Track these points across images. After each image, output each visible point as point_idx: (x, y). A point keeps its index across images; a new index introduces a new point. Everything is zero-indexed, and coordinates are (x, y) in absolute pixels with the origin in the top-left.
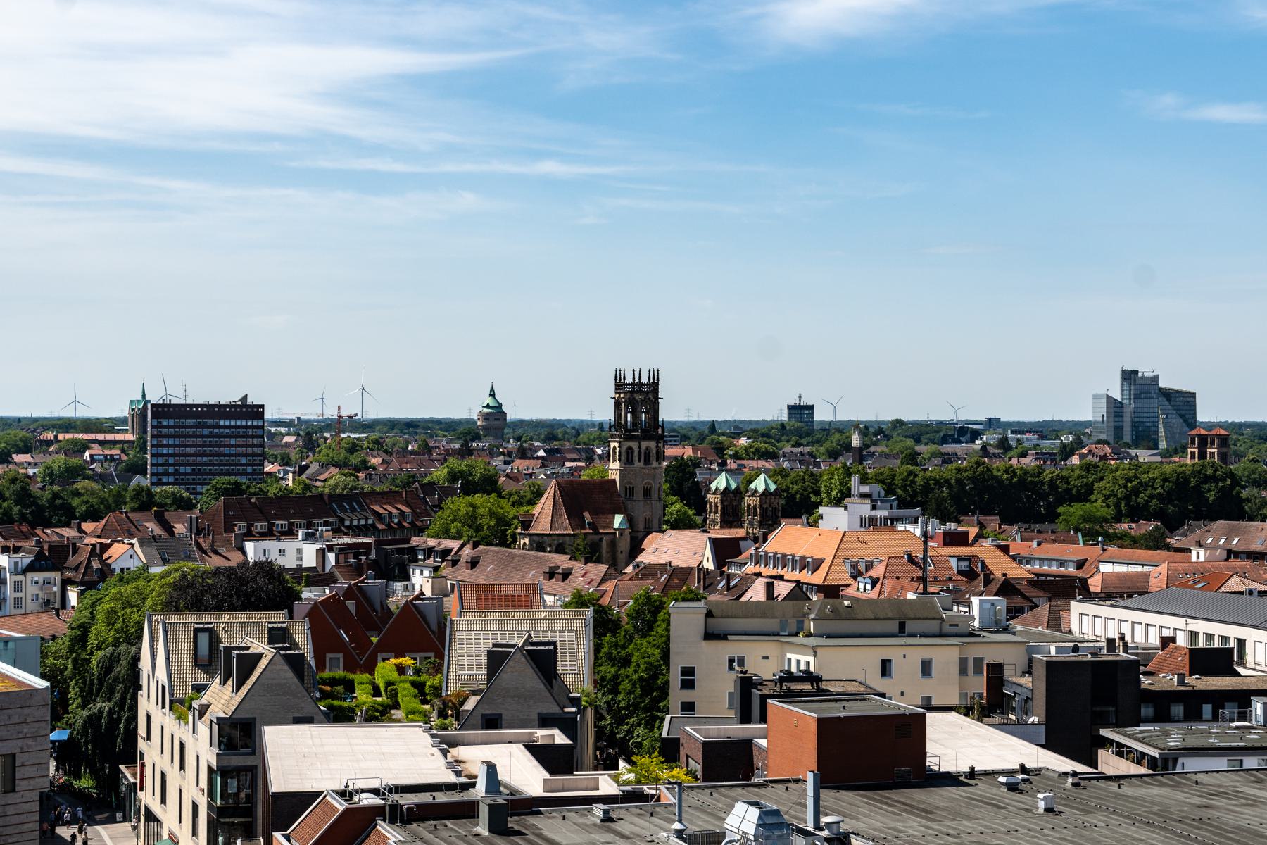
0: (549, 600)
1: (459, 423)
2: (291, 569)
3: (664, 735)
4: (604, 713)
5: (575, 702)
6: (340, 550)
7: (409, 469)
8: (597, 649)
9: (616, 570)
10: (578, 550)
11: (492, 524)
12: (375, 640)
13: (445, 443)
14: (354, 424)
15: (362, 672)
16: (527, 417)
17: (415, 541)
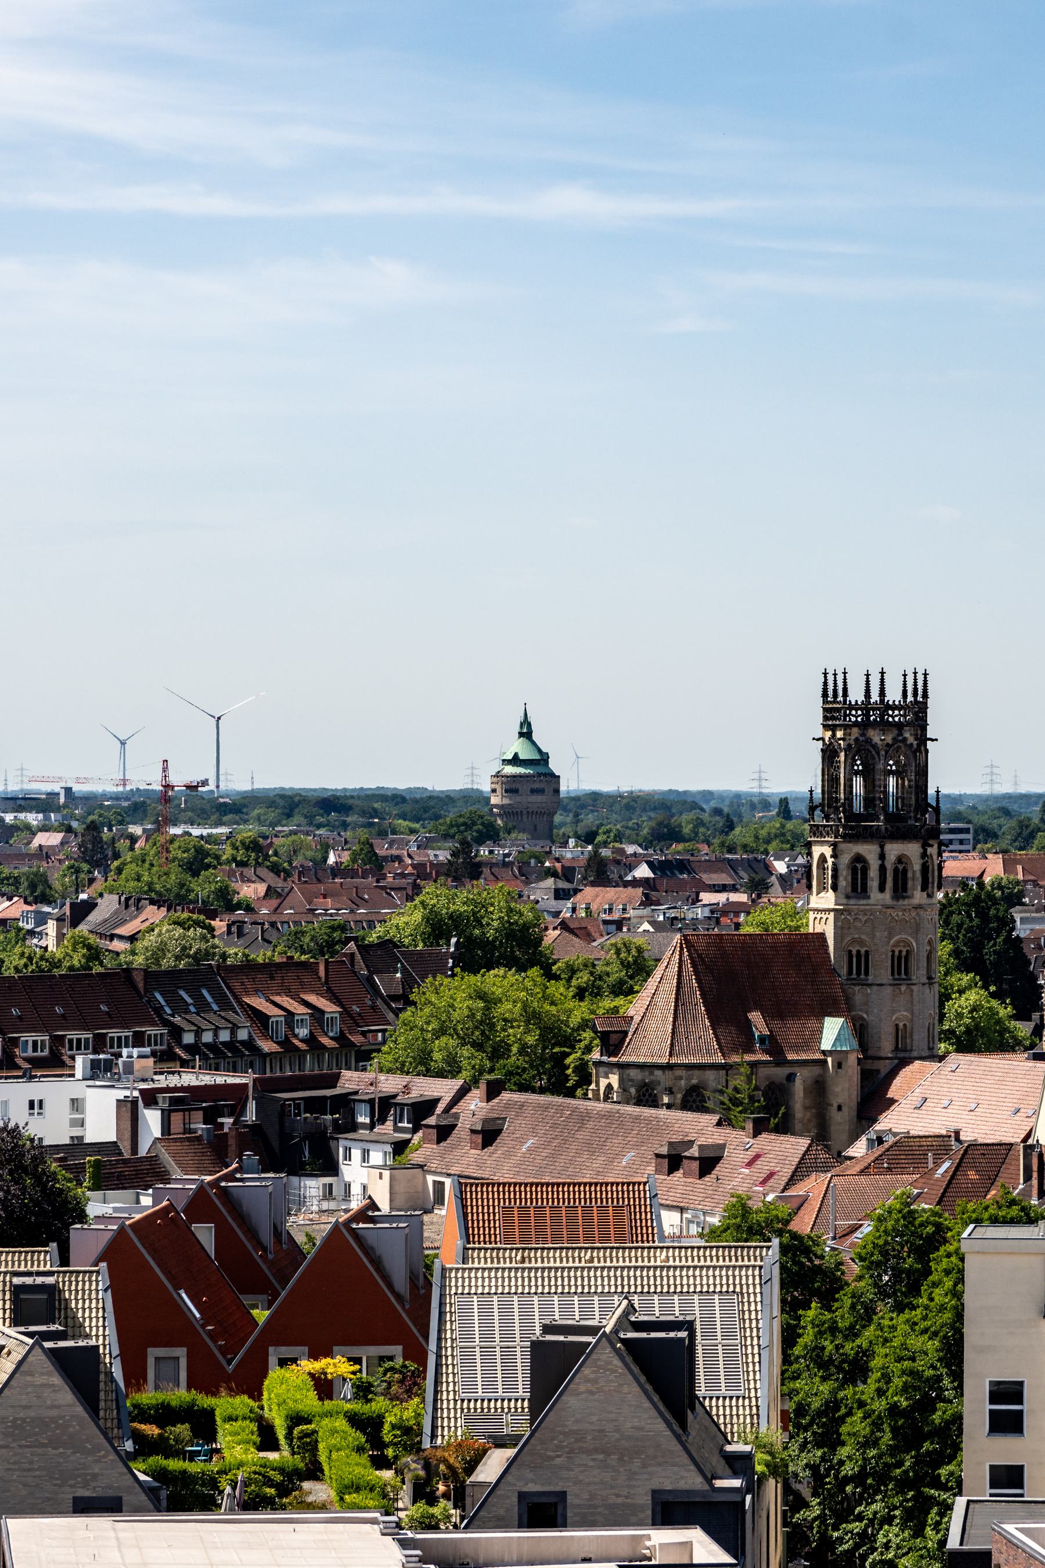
0: (670, 1221)
1: (447, 799)
2: (57, 1148)
3: (953, 1543)
4: (806, 1492)
5: (740, 1464)
6: (174, 1101)
7: (333, 910)
8: (789, 1336)
9: (827, 1148)
10: (735, 1102)
11: (531, 1040)
12: (261, 1315)
13: (411, 849)
14: (202, 804)
15: (233, 1392)
16: (606, 785)
17: (350, 1080)
